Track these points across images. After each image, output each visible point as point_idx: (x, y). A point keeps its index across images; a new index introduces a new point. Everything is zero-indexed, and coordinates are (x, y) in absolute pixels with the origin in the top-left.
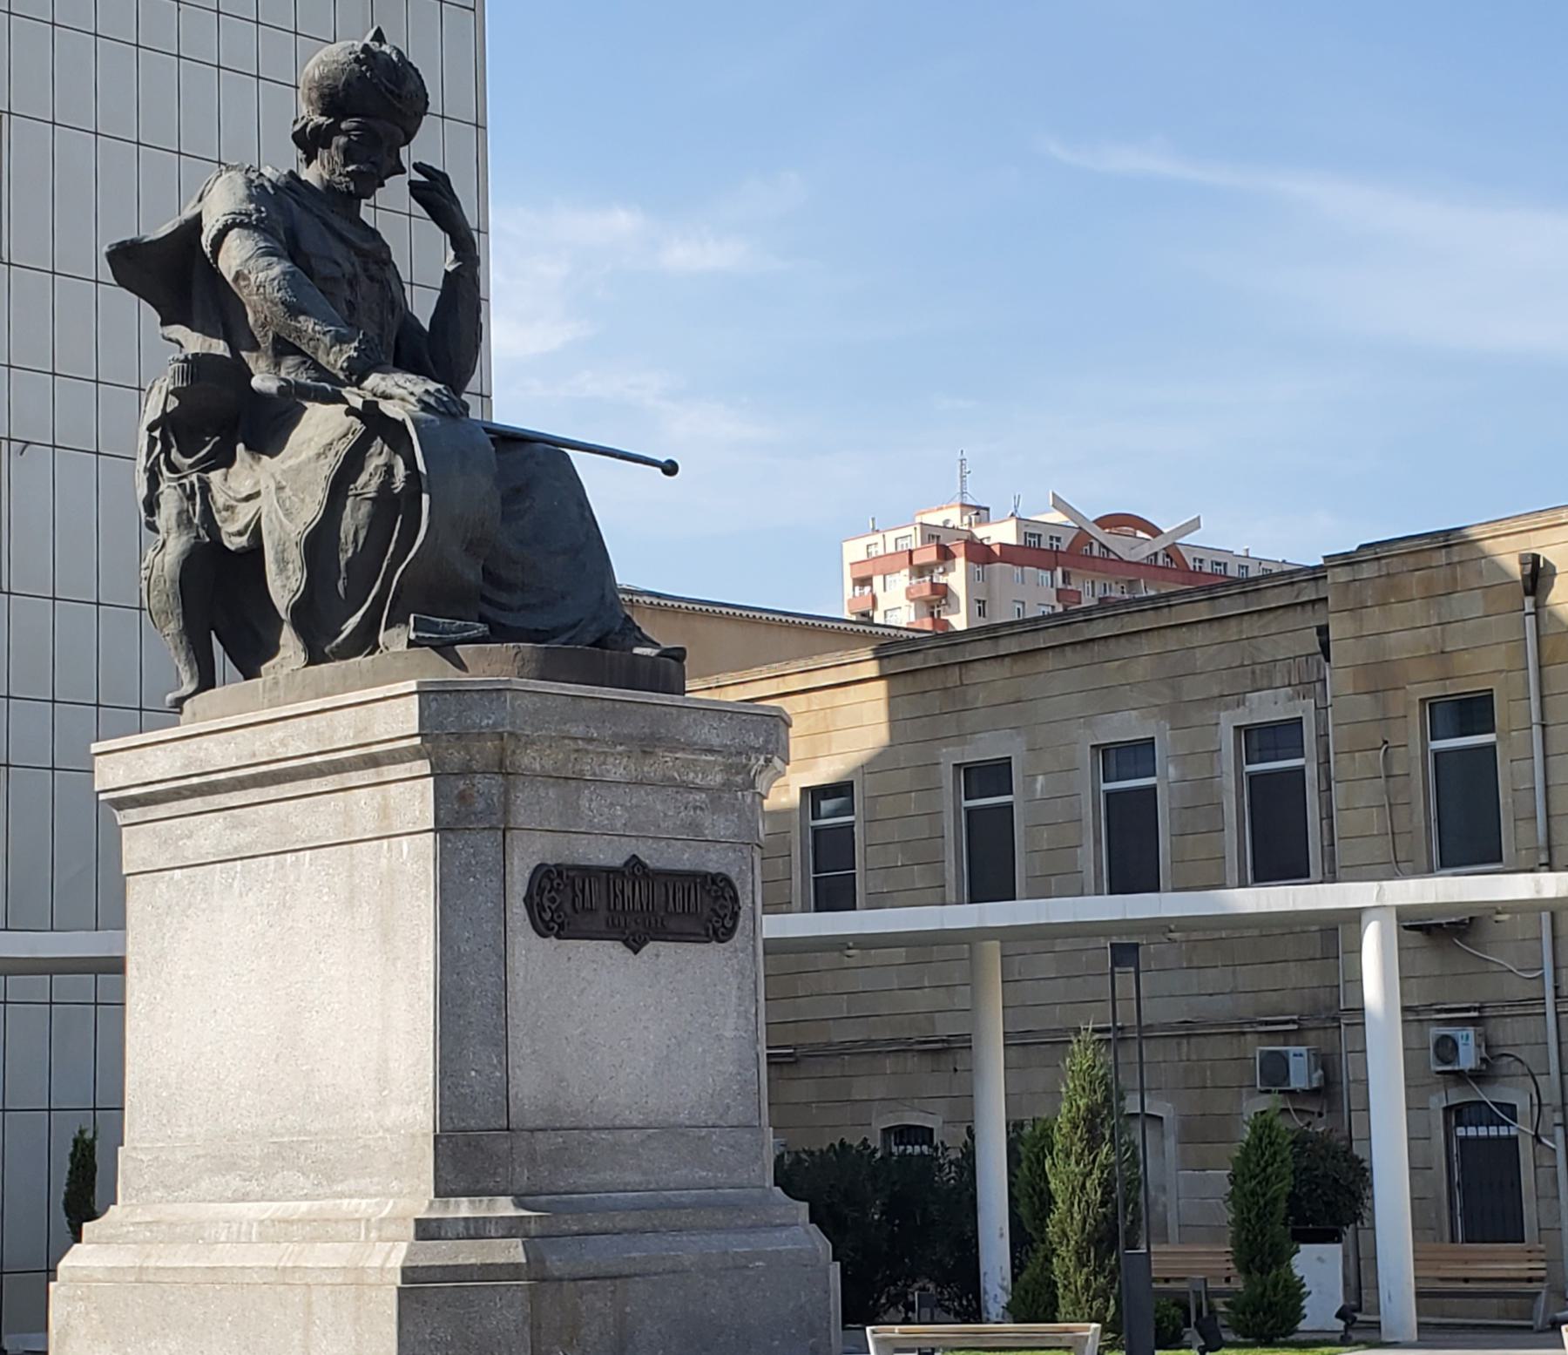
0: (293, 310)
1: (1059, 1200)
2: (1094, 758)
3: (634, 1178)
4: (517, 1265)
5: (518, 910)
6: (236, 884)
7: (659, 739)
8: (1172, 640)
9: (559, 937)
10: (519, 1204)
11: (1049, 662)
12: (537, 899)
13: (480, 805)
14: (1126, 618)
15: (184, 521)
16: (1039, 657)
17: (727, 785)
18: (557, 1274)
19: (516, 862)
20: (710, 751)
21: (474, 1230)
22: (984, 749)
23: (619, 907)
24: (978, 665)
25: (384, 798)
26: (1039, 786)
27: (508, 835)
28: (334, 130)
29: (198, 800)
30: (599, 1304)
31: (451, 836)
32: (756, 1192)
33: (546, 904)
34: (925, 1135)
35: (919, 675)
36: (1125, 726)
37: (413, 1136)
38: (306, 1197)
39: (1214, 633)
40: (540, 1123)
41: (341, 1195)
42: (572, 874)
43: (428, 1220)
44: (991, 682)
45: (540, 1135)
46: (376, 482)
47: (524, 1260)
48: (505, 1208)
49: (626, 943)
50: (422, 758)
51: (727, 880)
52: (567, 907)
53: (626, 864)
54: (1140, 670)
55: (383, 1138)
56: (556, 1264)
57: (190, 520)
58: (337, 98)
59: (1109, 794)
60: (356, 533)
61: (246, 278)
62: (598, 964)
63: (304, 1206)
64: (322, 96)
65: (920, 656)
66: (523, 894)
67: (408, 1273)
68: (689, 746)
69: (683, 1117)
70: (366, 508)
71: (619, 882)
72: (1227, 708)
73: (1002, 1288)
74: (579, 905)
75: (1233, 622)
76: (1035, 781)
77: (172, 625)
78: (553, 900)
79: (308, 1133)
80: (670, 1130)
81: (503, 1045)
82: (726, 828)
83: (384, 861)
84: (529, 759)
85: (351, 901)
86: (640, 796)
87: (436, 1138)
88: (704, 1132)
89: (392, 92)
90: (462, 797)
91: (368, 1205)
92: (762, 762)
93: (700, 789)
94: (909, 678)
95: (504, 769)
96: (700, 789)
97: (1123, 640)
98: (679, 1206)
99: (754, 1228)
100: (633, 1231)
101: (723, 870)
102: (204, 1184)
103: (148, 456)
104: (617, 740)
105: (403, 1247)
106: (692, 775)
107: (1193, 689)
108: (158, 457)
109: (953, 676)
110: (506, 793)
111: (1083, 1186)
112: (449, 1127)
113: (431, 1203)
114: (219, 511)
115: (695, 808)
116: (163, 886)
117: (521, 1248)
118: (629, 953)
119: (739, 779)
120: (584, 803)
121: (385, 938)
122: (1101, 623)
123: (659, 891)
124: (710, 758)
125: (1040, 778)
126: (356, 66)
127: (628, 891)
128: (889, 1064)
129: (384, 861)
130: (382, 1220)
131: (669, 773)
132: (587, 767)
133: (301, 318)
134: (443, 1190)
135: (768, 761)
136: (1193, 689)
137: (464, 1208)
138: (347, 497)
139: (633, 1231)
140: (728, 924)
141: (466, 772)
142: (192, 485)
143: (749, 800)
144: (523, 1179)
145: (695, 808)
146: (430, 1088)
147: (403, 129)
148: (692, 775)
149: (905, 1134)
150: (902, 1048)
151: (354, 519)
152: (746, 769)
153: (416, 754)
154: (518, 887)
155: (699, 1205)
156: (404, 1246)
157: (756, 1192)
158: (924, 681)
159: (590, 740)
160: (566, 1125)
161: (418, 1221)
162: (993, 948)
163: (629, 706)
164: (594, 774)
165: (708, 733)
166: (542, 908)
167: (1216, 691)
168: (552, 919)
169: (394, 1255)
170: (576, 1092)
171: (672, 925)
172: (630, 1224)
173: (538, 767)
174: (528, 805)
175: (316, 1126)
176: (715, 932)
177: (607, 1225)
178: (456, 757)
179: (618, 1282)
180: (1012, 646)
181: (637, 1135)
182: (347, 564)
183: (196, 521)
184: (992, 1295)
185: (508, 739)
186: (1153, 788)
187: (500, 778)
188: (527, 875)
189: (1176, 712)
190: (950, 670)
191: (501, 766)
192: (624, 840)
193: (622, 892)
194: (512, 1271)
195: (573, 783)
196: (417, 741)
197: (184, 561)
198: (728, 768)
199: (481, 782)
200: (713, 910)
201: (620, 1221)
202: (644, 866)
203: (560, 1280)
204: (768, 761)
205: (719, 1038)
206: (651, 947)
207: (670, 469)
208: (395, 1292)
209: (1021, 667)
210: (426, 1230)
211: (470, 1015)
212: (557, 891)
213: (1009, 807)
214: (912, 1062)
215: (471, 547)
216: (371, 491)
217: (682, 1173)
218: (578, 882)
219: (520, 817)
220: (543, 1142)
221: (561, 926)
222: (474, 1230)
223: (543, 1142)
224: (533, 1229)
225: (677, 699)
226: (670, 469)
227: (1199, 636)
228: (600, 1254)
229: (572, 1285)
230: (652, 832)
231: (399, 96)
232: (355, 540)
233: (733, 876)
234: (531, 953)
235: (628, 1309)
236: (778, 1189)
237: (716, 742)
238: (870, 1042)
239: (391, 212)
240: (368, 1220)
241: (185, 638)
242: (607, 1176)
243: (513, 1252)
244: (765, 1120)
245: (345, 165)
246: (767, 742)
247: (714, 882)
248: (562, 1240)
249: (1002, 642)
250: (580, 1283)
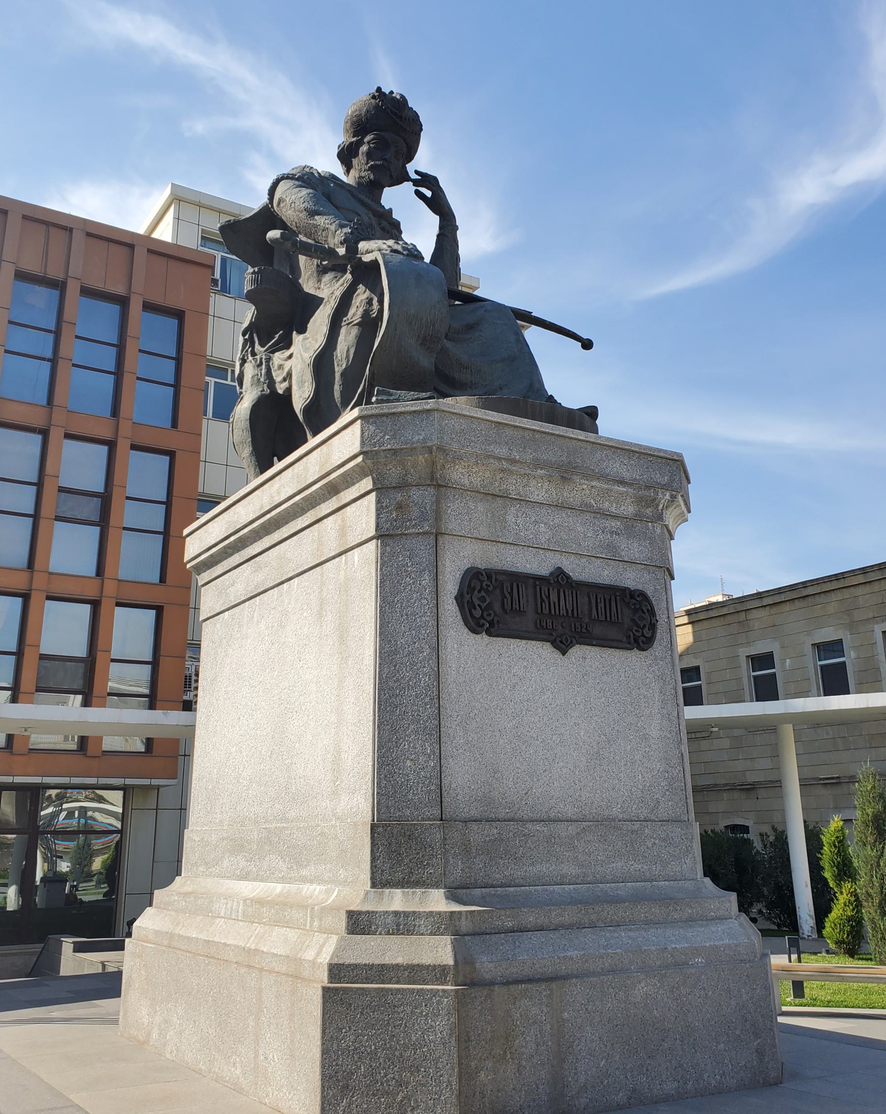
0: (312, 213)
1: (862, 873)
2: (814, 653)
3: (570, 870)
4: (444, 968)
5: (450, 609)
6: (256, 614)
7: (575, 468)
8: (846, 594)
9: (489, 634)
10: (453, 896)
11: (787, 607)
12: (467, 597)
13: (415, 513)
14: (823, 585)
15: (256, 381)
16: (783, 605)
17: (638, 517)
18: (488, 976)
19: (448, 564)
20: (622, 482)
21: (403, 924)
22: (760, 648)
23: (546, 611)
24: (754, 611)
25: (343, 520)
26: (787, 664)
27: (439, 538)
28: (359, 143)
29: (237, 555)
30: (534, 1011)
31: (390, 542)
32: (688, 885)
33: (476, 602)
34: (745, 829)
35: (726, 617)
36: (827, 634)
37: (355, 824)
38: (283, 880)
39: (867, 589)
40: (474, 813)
41: (304, 880)
42: (500, 578)
43: (360, 913)
44: (760, 618)
45: (474, 826)
46: (361, 310)
47: (451, 962)
48: (437, 901)
49: (554, 644)
50: (366, 476)
51: (643, 595)
52: (497, 606)
53: (551, 574)
54: (832, 608)
55: (334, 826)
56: (487, 965)
57: (259, 380)
58: (360, 126)
59: (822, 667)
60: (348, 351)
61: (284, 201)
62: (526, 663)
63: (279, 888)
64: (353, 123)
65: (726, 608)
66: (455, 592)
67: (336, 971)
68: (603, 477)
69: (616, 811)
70: (355, 331)
71: (545, 589)
72: (877, 623)
73: (810, 916)
74: (508, 607)
75: (876, 583)
76: (785, 662)
77: (246, 451)
78: (483, 599)
79: (286, 820)
80: (603, 824)
81: (438, 734)
82: (641, 552)
83: (342, 573)
84: (458, 474)
85: (320, 614)
86: (559, 518)
87: (373, 827)
88: (637, 825)
89: (395, 114)
90: (400, 507)
91: (320, 892)
92: (668, 497)
93: (615, 517)
94: (722, 618)
95: (438, 484)
96: (615, 517)
97: (822, 595)
98: (615, 900)
99: (690, 921)
100: (569, 927)
101: (640, 587)
102: (226, 863)
103: (242, 351)
104: (538, 464)
105: (332, 942)
106: (607, 504)
107: (859, 615)
108: (247, 351)
109: (742, 616)
110: (438, 502)
111: (878, 863)
112: (384, 816)
113: (367, 893)
114: (275, 371)
115: (612, 533)
116: (218, 626)
117: (449, 948)
118: (557, 654)
119: (649, 511)
120: (511, 518)
121: (342, 640)
122: (812, 588)
123: (583, 600)
124: (622, 489)
125: (788, 660)
126: (373, 101)
127: (554, 597)
128: (725, 795)
129: (342, 573)
130: (323, 909)
131: (587, 500)
132: (513, 486)
133: (316, 217)
134: (379, 881)
135: (673, 497)
136: (859, 615)
137: (397, 900)
138: (341, 327)
139: (569, 927)
140: (648, 634)
141: (403, 486)
142: (261, 359)
143: (658, 531)
144: (457, 872)
145: (612, 533)
146: (370, 776)
147: (405, 141)
148: (607, 504)
149: (735, 828)
150: (732, 788)
151: (347, 339)
152: (652, 502)
153: (359, 473)
154: (450, 586)
155: (637, 898)
156: (334, 939)
157: (688, 885)
158: (729, 619)
159: (513, 461)
160: (501, 816)
161: (351, 914)
162: (788, 732)
163: (548, 438)
164: (519, 494)
165: (618, 467)
166: (472, 606)
167: (871, 616)
168: (482, 617)
169: (323, 948)
170: (511, 784)
171: (597, 630)
172: (566, 918)
173: (467, 482)
174: (460, 514)
175: (292, 814)
176: (636, 640)
177: (543, 920)
178: (394, 473)
179: (554, 985)
180: (770, 601)
181: (572, 829)
182: (343, 374)
183: (262, 380)
184: (804, 919)
185: (438, 454)
186: (844, 663)
187: (432, 490)
188: (459, 576)
189: (852, 626)
190: (741, 614)
191: (432, 479)
192: (548, 554)
193: (549, 597)
194: (439, 973)
195: (500, 501)
196: (360, 459)
197: (254, 406)
198: (639, 500)
199: (416, 494)
200: (633, 620)
201: (556, 916)
202: (568, 577)
203: (492, 983)
204: (673, 497)
205: (646, 737)
206: (577, 651)
207: (587, 345)
208: (320, 992)
209: (774, 610)
210: (359, 923)
211: (407, 706)
212: (487, 591)
213: (774, 674)
214: (736, 795)
215: (427, 341)
216: (357, 319)
217: (618, 866)
218: (507, 585)
219: (452, 524)
220: (478, 834)
221: (491, 624)
222: (403, 924)
223: (478, 834)
224: (465, 925)
225: (591, 437)
226: (587, 345)
227: (860, 591)
228: (536, 953)
229: (504, 989)
230: (574, 548)
231: (401, 117)
232: (348, 357)
233: (649, 593)
234: (468, 654)
235: (566, 1015)
236: (708, 880)
237: (626, 475)
238: (716, 785)
239: (398, 199)
240: (313, 908)
241: (253, 458)
242: (543, 868)
243: (440, 951)
244: (692, 815)
245: (367, 164)
246: (671, 481)
247: (632, 597)
248: (495, 938)
249: (764, 599)
250: (512, 988)
